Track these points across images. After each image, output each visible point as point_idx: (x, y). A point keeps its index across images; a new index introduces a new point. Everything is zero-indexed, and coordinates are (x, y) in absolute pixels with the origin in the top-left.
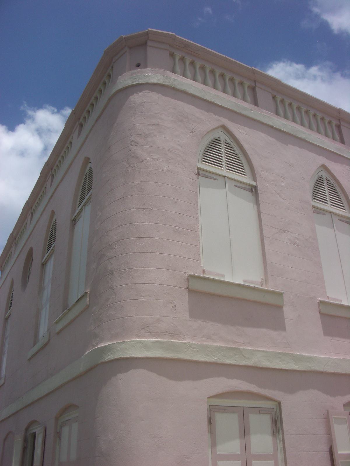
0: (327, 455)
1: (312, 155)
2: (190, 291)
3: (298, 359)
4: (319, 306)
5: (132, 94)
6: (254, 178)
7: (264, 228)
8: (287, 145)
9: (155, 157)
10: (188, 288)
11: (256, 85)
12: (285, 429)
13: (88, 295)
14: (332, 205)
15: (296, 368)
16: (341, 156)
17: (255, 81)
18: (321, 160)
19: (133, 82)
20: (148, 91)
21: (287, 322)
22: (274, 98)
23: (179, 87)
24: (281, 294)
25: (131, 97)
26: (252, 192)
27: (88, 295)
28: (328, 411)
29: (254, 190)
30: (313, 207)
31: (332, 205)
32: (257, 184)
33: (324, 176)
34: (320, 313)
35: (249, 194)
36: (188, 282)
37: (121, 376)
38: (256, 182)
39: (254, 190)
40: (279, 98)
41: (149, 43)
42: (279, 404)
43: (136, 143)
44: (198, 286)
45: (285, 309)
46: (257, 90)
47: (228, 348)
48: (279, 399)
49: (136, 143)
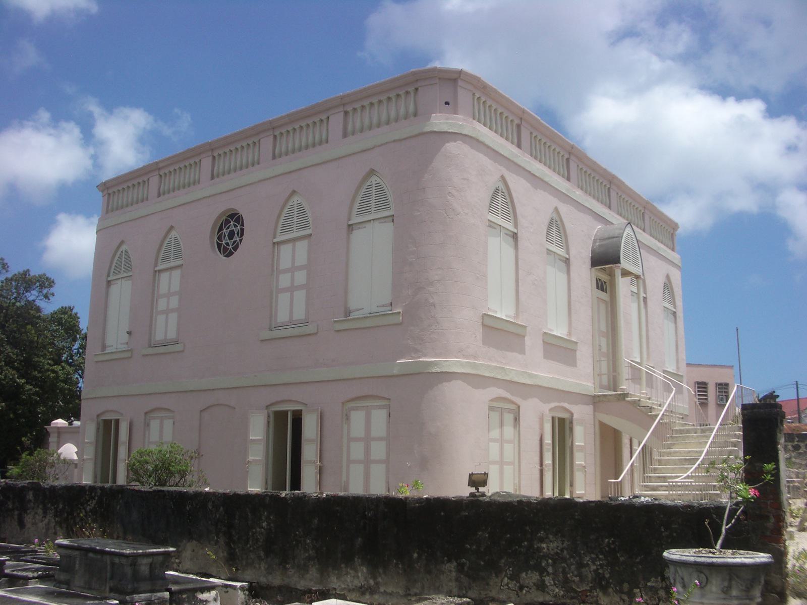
0: (538, 443)
1: (551, 198)
2: (484, 325)
3: (531, 376)
4: (543, 336)
5: (448, 142)
6: (516, 226)
7: (520, 272)
8: (536, 190)
9: (466, 212)
10: (482, 323)
11: (521, 123)
12: (521, 424)
13: (401, 314)
14: (502, 218)
15: (529, 382)
16: (567, 195)
17: (521, 119)
18: (554, 202)
19: (449, 129)
20: (461, 142)
21: (527, 348)
22: (531, 133)
23: (481, 139)
24: (525, 327)
25: (447, 144)
26: (514, 238)
27: (401, 314)
28: (543, 414)
29: (515, 236)
30: (548, 249)
31: (502, 218)
32: (569, 256)
33: (500, 188)
34: (544, 342)
35: (511, 239)
36: (483, 319)
37: (445, 384)
38: (569, 255)
39: (515, 236)
40: (534, 134)
41: (460, 83)
42: (519, 407)
43: (452, 195)
44: (488, 322)
45: (526, 338)
46: (522, 128)
47: (500, 367)
48: (519, 403)
49: (453, 196)
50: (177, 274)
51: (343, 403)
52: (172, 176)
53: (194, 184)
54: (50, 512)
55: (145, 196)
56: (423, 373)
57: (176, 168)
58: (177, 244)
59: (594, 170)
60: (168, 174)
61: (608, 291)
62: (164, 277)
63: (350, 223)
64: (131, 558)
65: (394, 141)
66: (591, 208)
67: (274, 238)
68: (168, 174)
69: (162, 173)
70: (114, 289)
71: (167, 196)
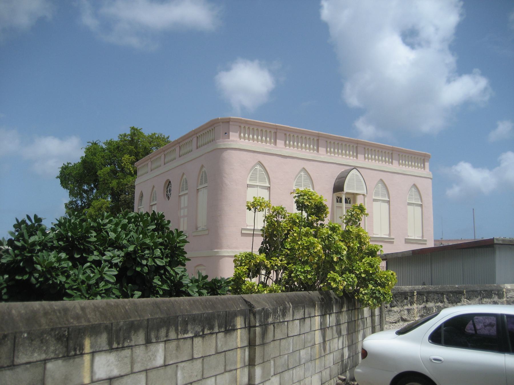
41: (231, 123)
50: (186, 197)
51: (195, 267)
52: (207, 135)
53: (213, 141)
54: (60, 313)
55: (213, 138)
56: (213, 256)
57: (208, 130)
58: (205, 174)
59: (342, 141)
60: (201, 136)
61: (351, 202)
62: (182, 198)
63: (198, 188)
64: (328, 353)
65: (208, 152)
66: (335, 162)
67: (179, 193)
68: (201, 136)
69: (198, 136)
70: (200, 193)
71: (190, 153)
